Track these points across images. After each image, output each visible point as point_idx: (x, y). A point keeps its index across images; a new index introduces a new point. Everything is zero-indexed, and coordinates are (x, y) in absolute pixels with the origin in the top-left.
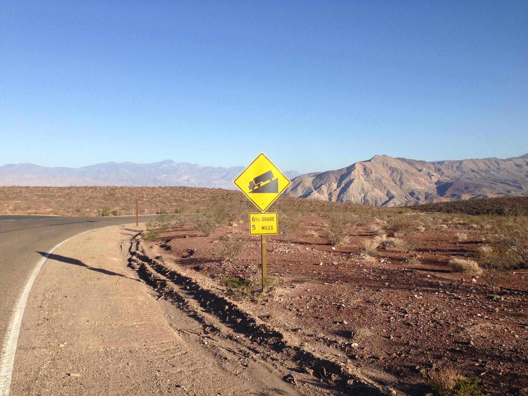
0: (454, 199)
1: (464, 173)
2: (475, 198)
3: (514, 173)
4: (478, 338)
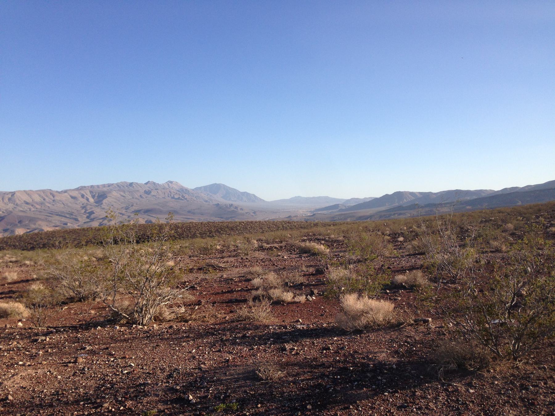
0: (7, 235)
1: (17, 205)
2: (30, 232)
3: (70, 204)
4: (17, 390)
